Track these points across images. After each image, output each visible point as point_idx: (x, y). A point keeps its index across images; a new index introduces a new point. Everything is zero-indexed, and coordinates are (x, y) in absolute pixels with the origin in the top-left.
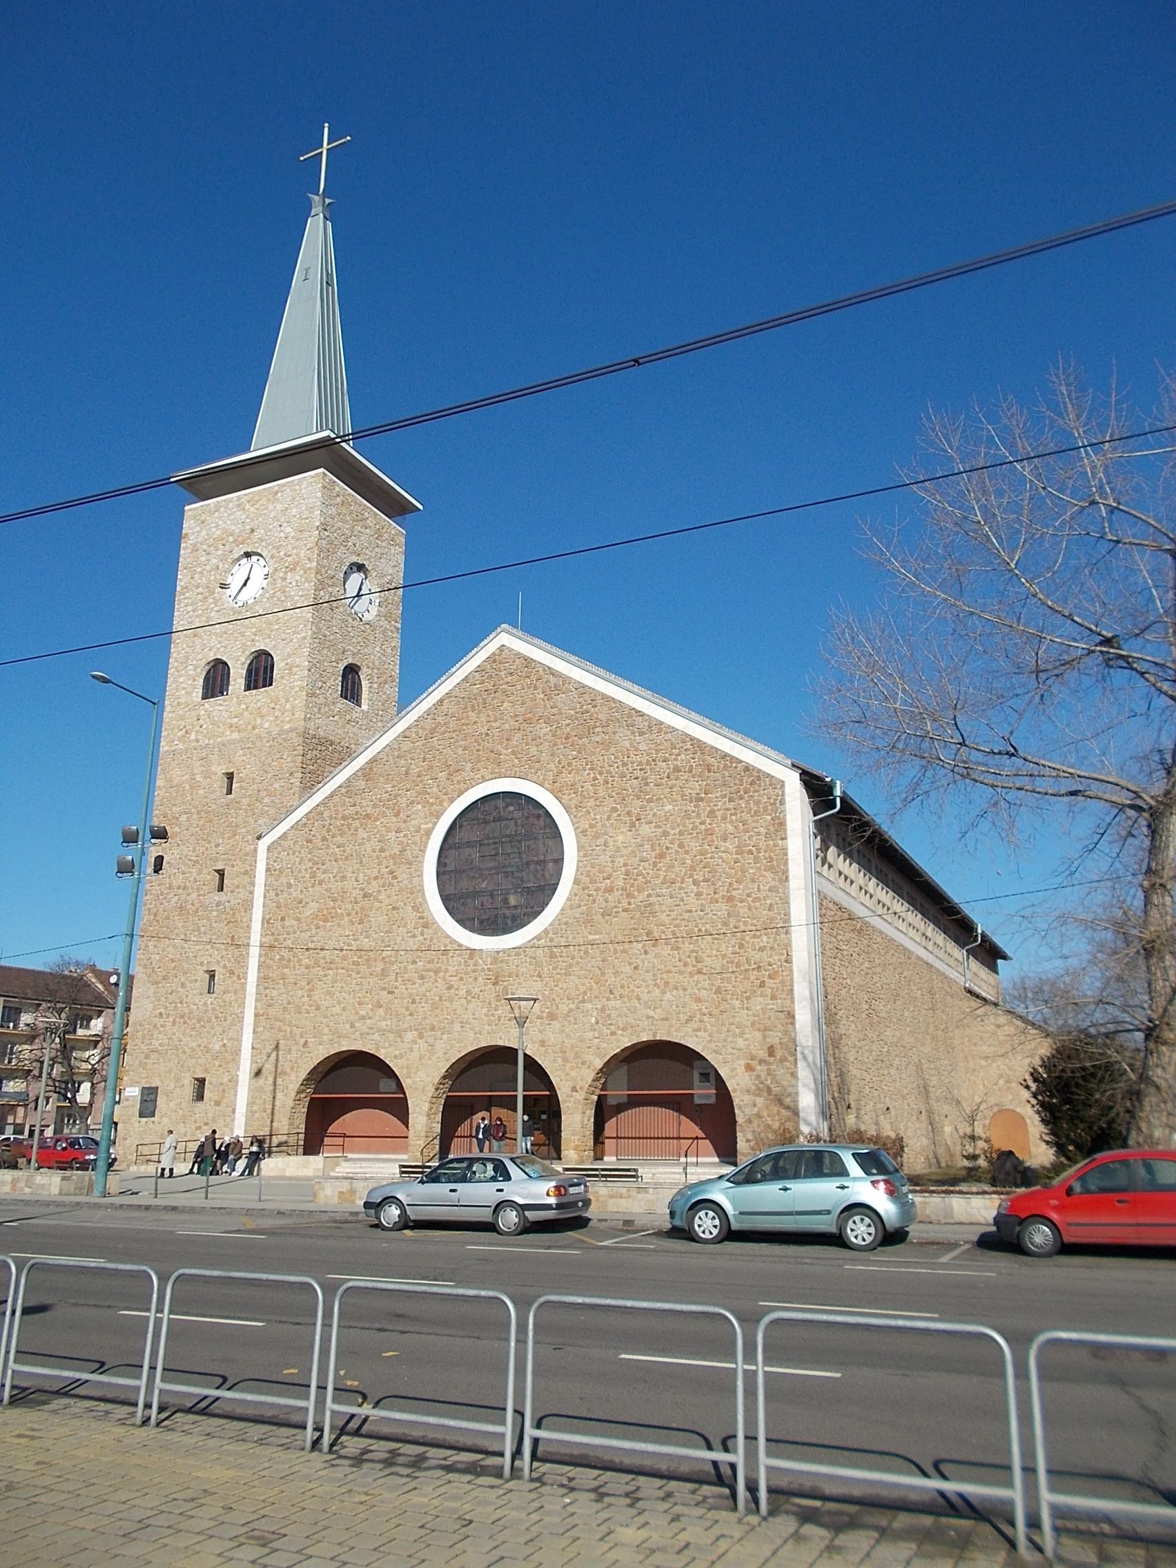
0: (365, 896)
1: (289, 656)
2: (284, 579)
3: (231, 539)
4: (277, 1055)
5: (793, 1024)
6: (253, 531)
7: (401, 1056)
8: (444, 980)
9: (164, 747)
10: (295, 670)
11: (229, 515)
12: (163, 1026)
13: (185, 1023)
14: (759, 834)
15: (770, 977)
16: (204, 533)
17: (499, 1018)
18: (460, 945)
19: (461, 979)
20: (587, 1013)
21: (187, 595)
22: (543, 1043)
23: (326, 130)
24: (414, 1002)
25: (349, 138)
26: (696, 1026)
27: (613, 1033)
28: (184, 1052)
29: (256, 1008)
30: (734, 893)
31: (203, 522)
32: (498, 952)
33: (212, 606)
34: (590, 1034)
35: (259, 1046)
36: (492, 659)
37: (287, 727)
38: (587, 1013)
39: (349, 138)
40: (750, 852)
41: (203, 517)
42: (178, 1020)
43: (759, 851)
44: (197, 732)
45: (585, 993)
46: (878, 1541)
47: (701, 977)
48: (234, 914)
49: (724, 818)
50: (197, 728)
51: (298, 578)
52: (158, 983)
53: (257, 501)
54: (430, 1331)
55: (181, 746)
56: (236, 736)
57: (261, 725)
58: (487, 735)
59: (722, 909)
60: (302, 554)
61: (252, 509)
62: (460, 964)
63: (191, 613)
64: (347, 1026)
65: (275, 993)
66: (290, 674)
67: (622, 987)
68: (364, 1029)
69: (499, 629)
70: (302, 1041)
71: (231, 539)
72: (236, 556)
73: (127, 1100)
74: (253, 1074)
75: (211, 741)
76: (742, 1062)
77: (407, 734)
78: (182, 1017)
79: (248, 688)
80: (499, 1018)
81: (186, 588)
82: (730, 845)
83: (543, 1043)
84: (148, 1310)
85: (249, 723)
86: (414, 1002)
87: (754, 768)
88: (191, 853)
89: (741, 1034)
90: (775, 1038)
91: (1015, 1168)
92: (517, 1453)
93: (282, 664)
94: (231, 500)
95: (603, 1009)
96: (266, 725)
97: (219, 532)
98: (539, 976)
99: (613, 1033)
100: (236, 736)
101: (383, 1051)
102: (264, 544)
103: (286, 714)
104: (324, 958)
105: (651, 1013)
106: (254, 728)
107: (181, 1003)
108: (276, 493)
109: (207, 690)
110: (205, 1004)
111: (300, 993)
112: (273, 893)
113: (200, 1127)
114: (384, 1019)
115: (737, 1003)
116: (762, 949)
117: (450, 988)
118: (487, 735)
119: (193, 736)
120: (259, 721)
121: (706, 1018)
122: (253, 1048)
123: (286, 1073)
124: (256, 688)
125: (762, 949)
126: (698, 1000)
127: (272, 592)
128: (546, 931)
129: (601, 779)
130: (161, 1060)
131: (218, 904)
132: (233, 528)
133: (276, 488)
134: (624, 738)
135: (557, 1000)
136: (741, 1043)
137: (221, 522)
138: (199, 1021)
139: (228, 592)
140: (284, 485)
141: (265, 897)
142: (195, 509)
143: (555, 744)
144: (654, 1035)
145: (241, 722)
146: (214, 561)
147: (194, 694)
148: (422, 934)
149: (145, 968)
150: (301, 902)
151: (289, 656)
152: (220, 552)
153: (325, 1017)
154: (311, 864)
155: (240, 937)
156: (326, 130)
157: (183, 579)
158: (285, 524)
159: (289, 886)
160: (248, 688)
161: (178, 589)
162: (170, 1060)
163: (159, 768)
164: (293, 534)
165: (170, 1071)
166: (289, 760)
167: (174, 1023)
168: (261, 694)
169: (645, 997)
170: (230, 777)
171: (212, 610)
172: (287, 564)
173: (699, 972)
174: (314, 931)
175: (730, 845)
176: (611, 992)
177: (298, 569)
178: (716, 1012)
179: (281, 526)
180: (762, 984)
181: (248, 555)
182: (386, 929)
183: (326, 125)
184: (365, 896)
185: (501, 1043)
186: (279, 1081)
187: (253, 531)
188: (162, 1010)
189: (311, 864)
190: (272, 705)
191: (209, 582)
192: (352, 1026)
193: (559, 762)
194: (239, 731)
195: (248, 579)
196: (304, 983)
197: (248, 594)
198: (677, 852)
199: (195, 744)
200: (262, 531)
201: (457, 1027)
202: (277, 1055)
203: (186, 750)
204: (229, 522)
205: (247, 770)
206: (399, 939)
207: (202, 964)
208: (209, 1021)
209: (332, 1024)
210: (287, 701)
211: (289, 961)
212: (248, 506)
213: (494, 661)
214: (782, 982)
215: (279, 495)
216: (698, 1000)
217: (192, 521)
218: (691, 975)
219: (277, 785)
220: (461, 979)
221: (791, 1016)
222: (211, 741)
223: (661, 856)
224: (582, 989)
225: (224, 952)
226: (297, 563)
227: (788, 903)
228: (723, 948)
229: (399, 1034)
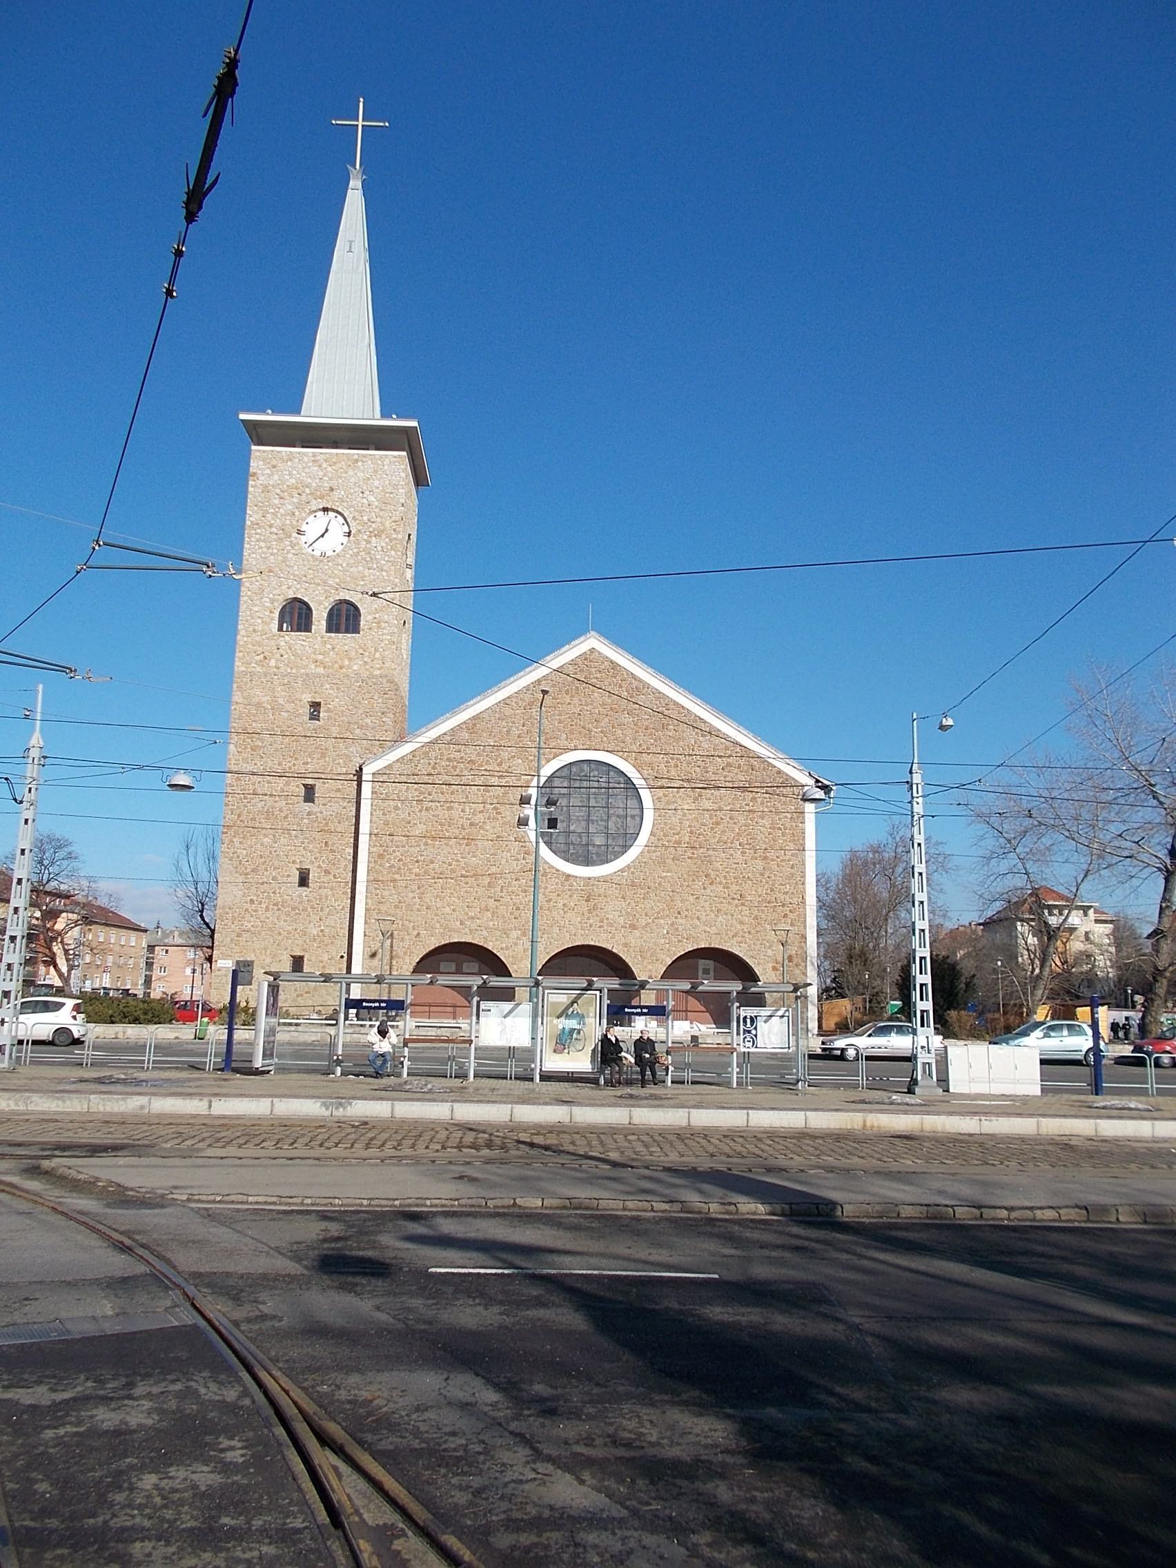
0: (471, 824)
1: (377, 611)
2: (368, 542)
4: (392, 942)
5: (805, 942)
6: (332, 489)
7: (507, 948)
8: (544, 894)
9: (239, 666)
10: (383, 625)
12: (256, 911)
13: (279, 909)
14: (786, 817)
15: (791, 911)
16: (276, 477)
17: (591, 926)
18: (557, 870)
19: (558, 895)
20: (661, 926)
21: (259, 531)
22: (626, 945)
23: (361, 105)
24: (518, 909)
25: (387, 124)
26: (739, 939)
27: (679, 941)
28: (280, 934)
29: (366, 904)
30: (768, 854)
31: (274, 467)
32: (589, 879)
33: (289, 548)
34: (663, 941)
35: (371, 934)
36: (584, 657)
37: (378, 672)
38: (661, 926)
39: (387, 124)
40: (781, 829)
41: (274, 462)
42: (271, 907)
43: (785, 829)
44: (277, 660)
45: (659, 913)
47: (744, 908)
48: (327, 824)
49: (762, 803)
50: (278, 656)
51: (383, 544)
52: (247, 874)
53: (335, 463)
55: (259, 669)
56: (321, 670)
57: (349, 667)
58: (579, 714)
59: (760, 864)
60: (387, 524)
61: (329, 469)
62: (557, 884)
63: (265, 550)
64: (458, 923)
65: (386, 893)
66: (379, 627)
67: (687, 910)
68: (474, 926)
69: (588, 635)
70: (415, 933)
71: (307, 491)
72: (314, 508)
73: (219, 970)
74: (366, 956)
75: (294, 671)
76: (771, 965)
77: (508, 702)
78: (276, 905)
79: (329, 630)
80: (591, 926)
82: (767, 822)
83: (626, 945)
85: (336, 662)
86: (518, 909)
87: (784, 773)
88: (276, 766)
89: (770, 947)
90: (792, 950)
92: (148, 1063)
93: (369, 618)
95: (672, 924)
96: (355, 667)
97: (293, 481)
98: (623, 897)
99: (679, 941)
100: (321, 670)
101: (491, 944)
102: (345, 504)
103: (376, 661)
104: (434, 869)
105: (708, 929)
106: (341, 668)
107: (274, 893)
108: (357, 461)
110: (300, 896)
111: (411, 895)
112: (380, 813)
113: (302, 995)
114: (492, 920)
115: (768, 927)
116: (786, 893)
117: (550, 900)
118: (579, 714)
119: (273, 663)
120: (347, 663)
121: (747, 935)
122: (365, 935)
123: (399, 957)
124: (338, 631)
125: (786, 893)
126: (741, 923)
127: (355, 550)
128: (628, 866)
129: (672, 763)
130: (255, 939)
131: (309, 814)
132: (309, 480)
133: (356, 457)
134: (690, 736)
135: (637, 916)
136: (770, 952)
137: (295, 472)
138: (293, 909)
139: (303, 538)
140: (364, 456)
141: (372, 814)
142: (264, 452)
143: (637, 732)
144: (710, 944)
145: (327, 660)
146: (290, 507)
147: (272, 625)
148: (524, 859)
149: (231, 860)
150: (409, 823)
151: (377, 611)
152: (295, 500)
153: (436, 915)
154: (417, 793)
155: (334, 844)
156: (361, 105)
157: (252, 515)
158: (367, 492)
159: (396, 808)
160: (329, 630)
161: (248, 523)
162: (264, 940)
163: (235, 686)
164: (377, 503)
165: (265, 949)
166: (380, 701)
167: (267, 909)
168: (344, 640)
169: (703, 918)
170: (316, 706)
171: (288, 552)
172: (371, 529)
173: (743, 904)
174: (423, 847)
175: (767, 822)
176: (679, 913)
177: (383, 537)
178: (753, 931)
180: (785, 916)
181: (325, 510)
182: (492, 851)
183: (362, 100)
184: (471, 824)
185: (592, 943)
186: (394, 962)
187: (332, 489)
188: (255, 898)
189: (417, 793)
190: (361, 651)
191: (284, 525)
192: (462, 923)
193: (640, 745)
194: (325, 667)
195: (327, 530)
196: (415, 887)
197: (321, 546)
198: (728, 822)
199: (275, 670)
201: (556, 930)
202: (392, 942)
203: (265, 675)
205: (334, 701)
206: (503, 861)
207: (294, 862)
208: (305, 910)
209: (443, 921)
210: (376, 650)
211: (399, 869)
212: (325, 465)
213: (586, 659)
214: (798, 915)
215: (360, 463)
216: (741, 923)
217: (261, 463)
218: (737, 906)
219: (368, 721)
220: (558, 895)
221: (804, 937)
222: (294, 671)
223: (717, 823)
224: (657, 910)
225: (318, 855)
226: (383, 531)
227: (804, 864)
228: (760, 890)
229: (506, 933)
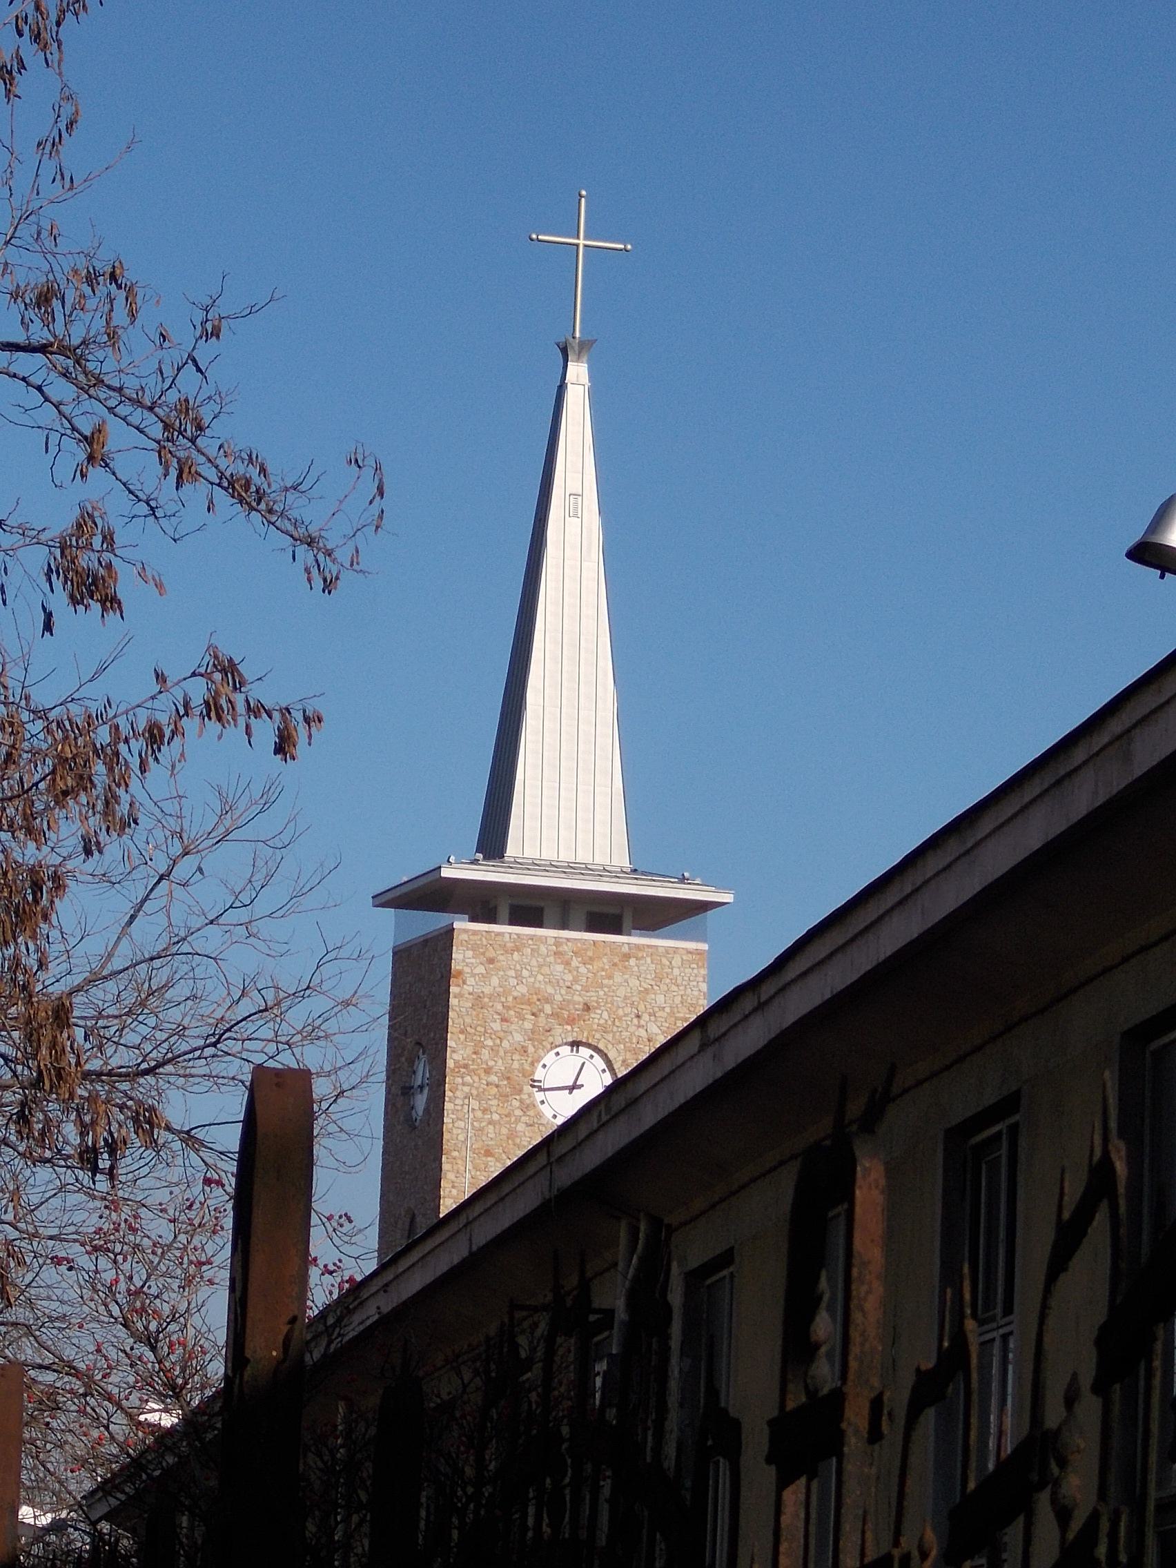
3: (548, 1009)
6: (587, 1008)
11: (540, 966)
31: (491, 961)
46: (544, 1199)
54: (522, 1179)
61: (583, 970)
81: (466, 1066)
84: (577, 245)
91: (394, 1000)
94: (544, 940)
97: (522, 989)
102: (610, 1037)
108: (627, 957)
109: (522, 613)
133: (625, 949)
146: (518, 1037)
179: (638, 1016)
200: (605, 1015)
204: (540, 977)
